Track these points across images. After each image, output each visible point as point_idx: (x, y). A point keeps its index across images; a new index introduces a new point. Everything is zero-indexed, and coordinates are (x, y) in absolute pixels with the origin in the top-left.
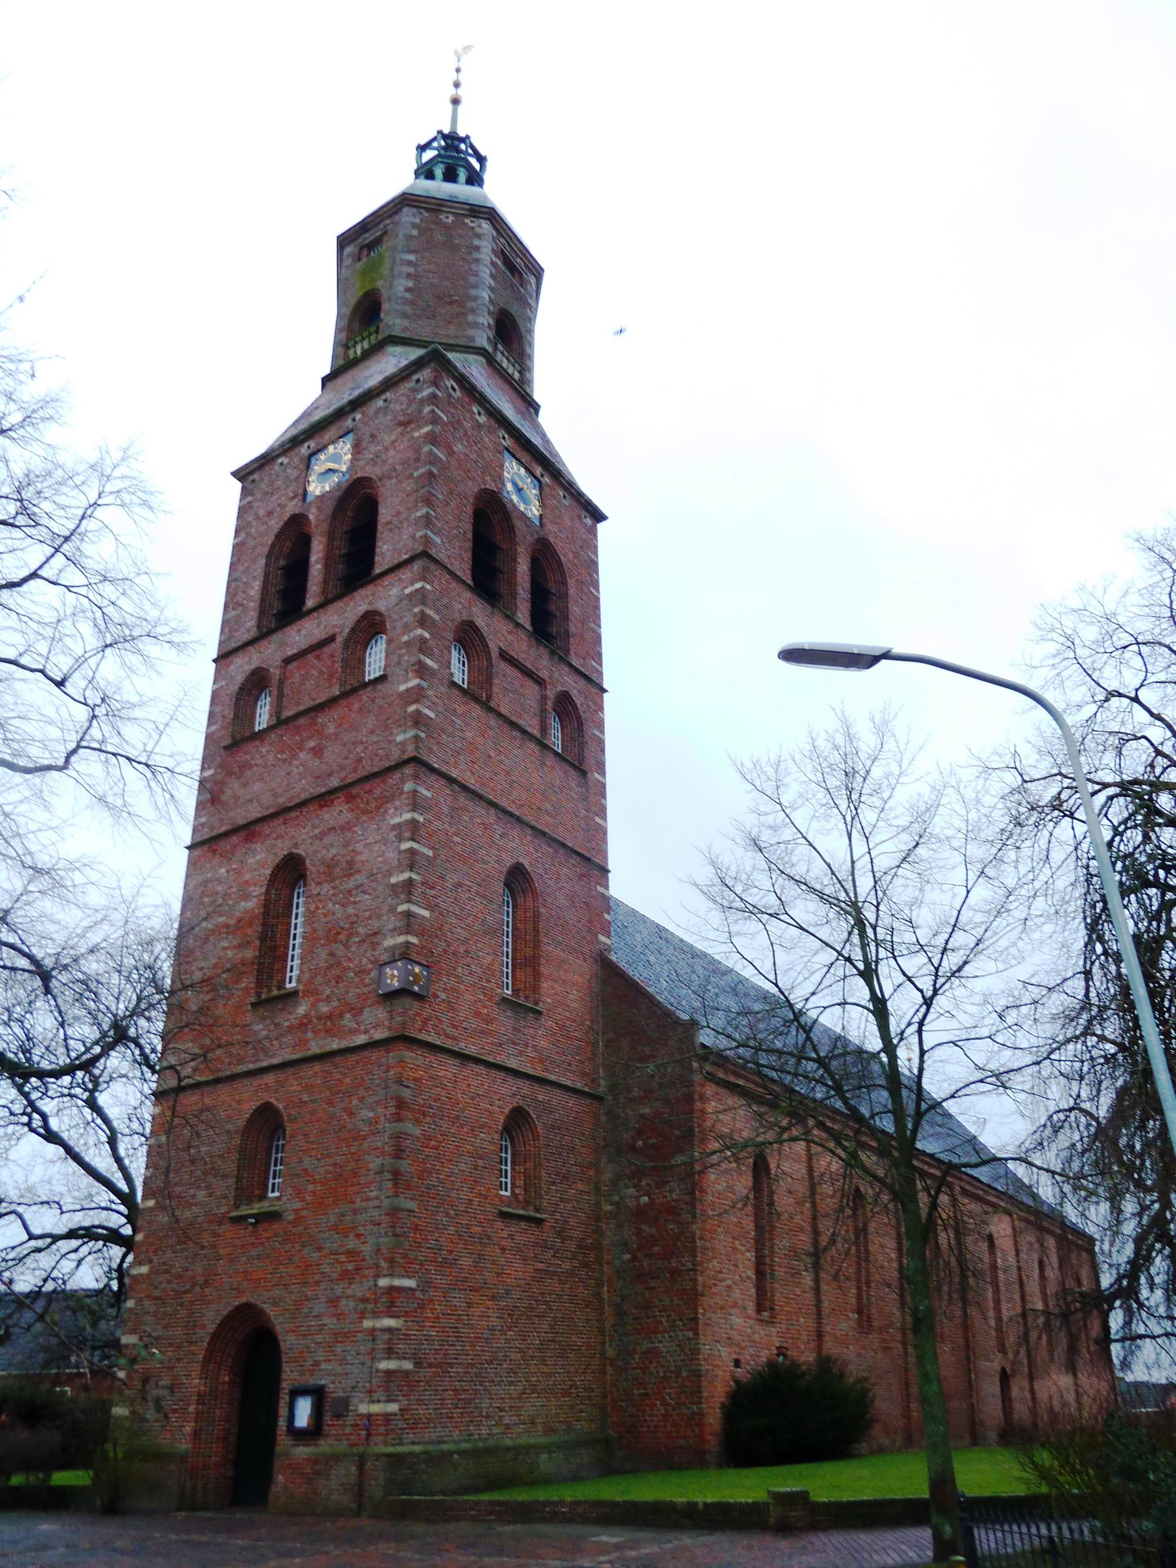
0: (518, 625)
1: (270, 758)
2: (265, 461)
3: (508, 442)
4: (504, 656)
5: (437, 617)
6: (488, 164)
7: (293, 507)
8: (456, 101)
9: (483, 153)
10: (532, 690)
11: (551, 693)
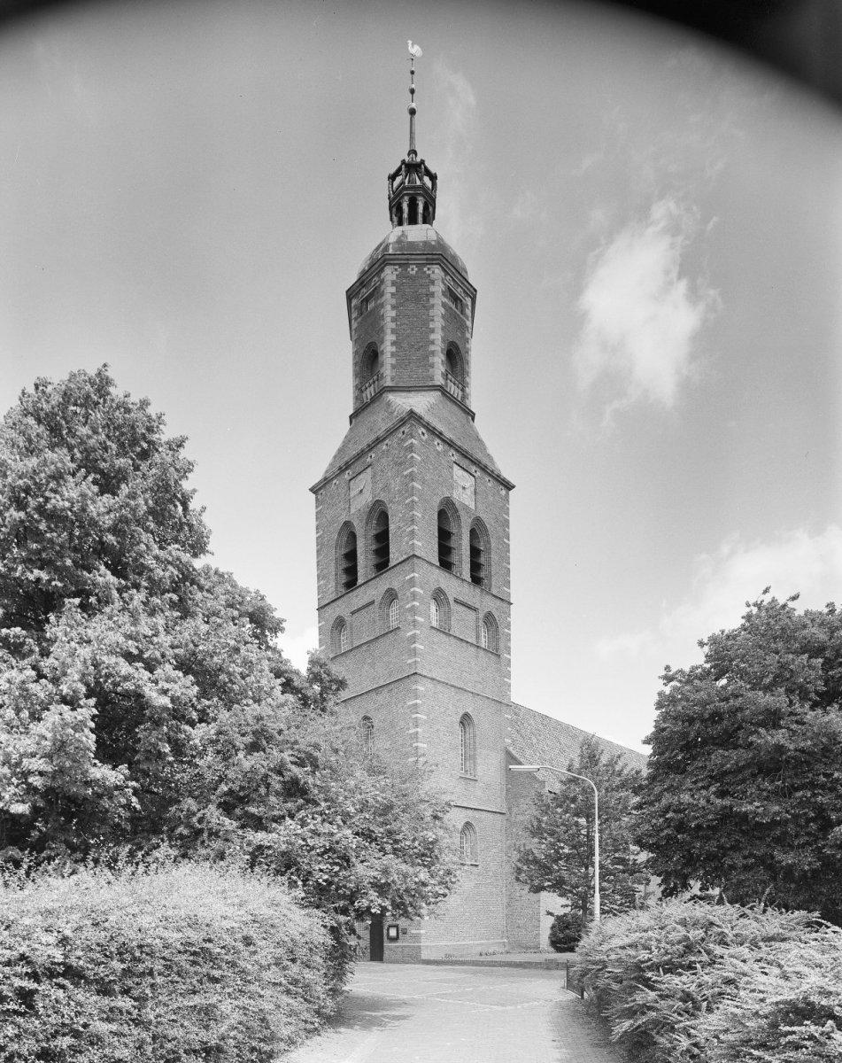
0: (463, 580)
1: (351, 666)
2: (326, 481)
3: (456, 457)
4: (456, 601)
5: (422, 592)
6: (438, 182)
7: (343, 518)
8: (413, 112)
9: (433, 171)
10: (472, 615)
11: (481, 616)
